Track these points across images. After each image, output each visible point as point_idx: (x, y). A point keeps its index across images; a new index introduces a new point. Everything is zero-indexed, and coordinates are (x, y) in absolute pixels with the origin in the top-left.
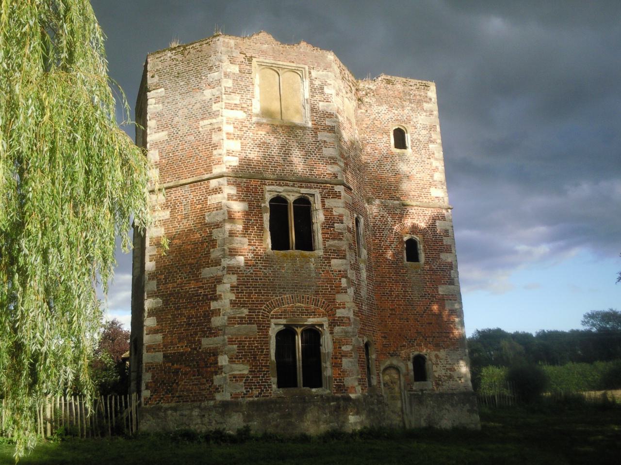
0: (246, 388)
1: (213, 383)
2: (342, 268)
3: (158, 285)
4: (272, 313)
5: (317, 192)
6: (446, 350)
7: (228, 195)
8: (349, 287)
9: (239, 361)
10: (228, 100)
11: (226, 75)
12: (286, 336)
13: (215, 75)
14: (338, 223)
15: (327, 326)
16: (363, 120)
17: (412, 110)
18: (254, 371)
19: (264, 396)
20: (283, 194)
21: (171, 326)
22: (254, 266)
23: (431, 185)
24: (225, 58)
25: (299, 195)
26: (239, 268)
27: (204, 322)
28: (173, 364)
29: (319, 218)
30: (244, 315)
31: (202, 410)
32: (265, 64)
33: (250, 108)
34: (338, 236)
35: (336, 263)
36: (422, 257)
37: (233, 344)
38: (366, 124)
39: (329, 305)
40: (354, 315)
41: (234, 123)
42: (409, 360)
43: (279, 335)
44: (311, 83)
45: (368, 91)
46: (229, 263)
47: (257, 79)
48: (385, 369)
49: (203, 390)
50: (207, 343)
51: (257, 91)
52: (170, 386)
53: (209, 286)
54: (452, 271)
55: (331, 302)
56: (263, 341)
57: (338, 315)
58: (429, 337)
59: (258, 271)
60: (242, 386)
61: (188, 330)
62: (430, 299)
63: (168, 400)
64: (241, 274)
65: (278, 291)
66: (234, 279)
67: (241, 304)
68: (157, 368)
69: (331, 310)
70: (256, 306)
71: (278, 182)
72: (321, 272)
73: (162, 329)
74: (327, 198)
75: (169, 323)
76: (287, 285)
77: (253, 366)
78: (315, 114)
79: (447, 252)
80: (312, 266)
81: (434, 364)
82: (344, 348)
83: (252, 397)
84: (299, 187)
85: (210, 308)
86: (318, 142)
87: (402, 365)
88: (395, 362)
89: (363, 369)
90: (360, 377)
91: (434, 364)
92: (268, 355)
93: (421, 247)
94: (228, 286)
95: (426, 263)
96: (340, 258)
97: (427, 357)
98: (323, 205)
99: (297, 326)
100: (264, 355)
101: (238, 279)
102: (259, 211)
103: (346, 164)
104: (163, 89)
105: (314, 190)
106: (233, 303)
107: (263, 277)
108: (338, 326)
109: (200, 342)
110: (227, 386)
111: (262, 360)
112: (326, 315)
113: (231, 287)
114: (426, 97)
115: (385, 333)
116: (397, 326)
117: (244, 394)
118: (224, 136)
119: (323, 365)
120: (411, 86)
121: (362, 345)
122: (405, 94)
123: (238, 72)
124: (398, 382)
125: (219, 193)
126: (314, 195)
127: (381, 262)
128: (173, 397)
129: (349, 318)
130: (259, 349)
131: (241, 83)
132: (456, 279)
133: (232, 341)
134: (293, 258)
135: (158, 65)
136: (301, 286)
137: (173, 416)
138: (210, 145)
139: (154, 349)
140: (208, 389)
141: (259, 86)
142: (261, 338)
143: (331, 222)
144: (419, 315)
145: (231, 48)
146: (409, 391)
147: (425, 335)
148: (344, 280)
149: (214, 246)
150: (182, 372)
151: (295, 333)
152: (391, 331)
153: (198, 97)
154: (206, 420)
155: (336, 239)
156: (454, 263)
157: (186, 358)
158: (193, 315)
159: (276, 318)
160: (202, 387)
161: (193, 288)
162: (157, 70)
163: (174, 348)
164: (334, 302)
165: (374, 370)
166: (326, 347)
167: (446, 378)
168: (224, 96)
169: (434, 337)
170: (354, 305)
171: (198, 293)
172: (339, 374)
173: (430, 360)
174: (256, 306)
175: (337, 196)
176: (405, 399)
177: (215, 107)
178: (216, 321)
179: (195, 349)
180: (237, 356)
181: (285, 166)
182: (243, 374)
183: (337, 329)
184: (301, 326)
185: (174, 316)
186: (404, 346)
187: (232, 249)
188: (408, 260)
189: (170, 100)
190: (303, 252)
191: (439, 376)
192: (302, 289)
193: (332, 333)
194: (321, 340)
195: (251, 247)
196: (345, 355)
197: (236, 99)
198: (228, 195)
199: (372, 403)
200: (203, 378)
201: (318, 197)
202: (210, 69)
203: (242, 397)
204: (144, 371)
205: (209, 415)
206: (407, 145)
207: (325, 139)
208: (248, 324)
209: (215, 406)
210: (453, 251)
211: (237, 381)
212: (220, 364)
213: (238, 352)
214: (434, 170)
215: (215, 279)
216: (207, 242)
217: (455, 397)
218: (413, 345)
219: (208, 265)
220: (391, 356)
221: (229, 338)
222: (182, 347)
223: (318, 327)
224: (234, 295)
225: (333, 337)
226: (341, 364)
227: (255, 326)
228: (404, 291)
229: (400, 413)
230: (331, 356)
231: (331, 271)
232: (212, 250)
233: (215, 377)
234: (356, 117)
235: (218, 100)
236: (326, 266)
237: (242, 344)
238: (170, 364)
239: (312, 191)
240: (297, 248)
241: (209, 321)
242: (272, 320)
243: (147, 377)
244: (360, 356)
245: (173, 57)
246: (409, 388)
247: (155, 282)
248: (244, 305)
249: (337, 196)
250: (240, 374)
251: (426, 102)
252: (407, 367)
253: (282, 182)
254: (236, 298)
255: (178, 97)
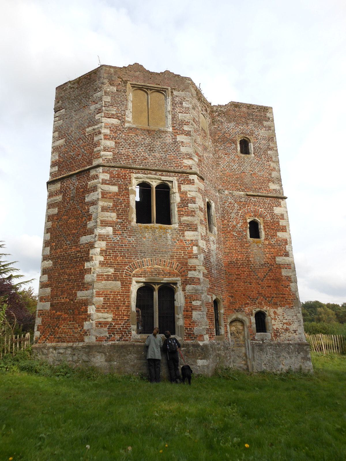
0: (109, 333)
1: (83, 328)
2: (194, 238)
3: (51, 250)
4: (134, 272)
5: (174, 179)
6: (283, 308)
7: (103, 180)
8: (200, 254)
9: (104, 311)
10: (107, 111)
11: (106, 93)
12: (145, 291)
13: (99, 94)
14: (191, 203)
15: (180, 284)
16: (216, 133)
17: (255, 127)
18: (117, 319)
19: (124, 340)
20: (148, 181)
21: (57, 282)
22: (120, 235)
23: (269, 181)
24: (106, 81)
25: (161, 181)
26: (108, 236)
27: (79, 279)
28: (56, 312)
29: (176, 198)
30: (110, 274)
31: (73, 349)
32: (137, 86)
33: (124, 117)
34: (192, 213)
35: (189, 235)
36: (263, 234)
37: (99, 297)
38: (219, 136)
39: (182, 268)
40: (203, 276)
41: (110, 128)
42: (252, 315)
43: (140, 290)
44: (173, 99)
45: (220, 112)
46: (100, 232)
47: (131, 97)
48: (231, 322)
49: (76, 333)
50: (81, 295)
51: (130, 105)
52: (54, 329)
53: (84, 250)
54: (287, 246)
55: (183, 265)
56: (125, 295)
57: (189, 276)
58: (268, 297)
59: (124, 239)
60: (105, 331)
61: (68, 285)
62: (269, 267)
63: (51, 340)
64: (110, 240)
65: (140, 255)
66: (103, 244)
67: (108, 264)
68: (46, 315)
69: (184, 271)
70: (120, 267)
71: (143, 171)
72: (176, 241)
73: (51, 285)
74: (183, 184)
75: (56, 280)
76: (147, 251)
77: (116, 315)
78: (175, 122)
79: (283, 232)
80: (169, 237)
81: (273, 319)
82: (194, 303)
83: (114, 340)
84: (160, 175)
85: (84, 267)
86: (177, 142)
87: (245, 319)
88: (240, 316)
89: (211, 321)
90: (208, 327)
91: (273, 319)
92: (129, 306)
93: (261, 227)
94: (98, 250)
95: (266, 239)
96: (192, 231)
97: (267, 313)
98: (180, 189)
99: (155, 283)
100: (126, 306)
101: (106, 245)
102: (127, 192)
103: (200, 160)
104: (64, 110)
105: (172, 178)
106: (102, 264)
107: (127, 243)
108: (190, 284)
109: (76, 294)
110: (93, 331)
111: (124, 310)
112: (179, 275)
113: (101, 251)
114: (266, 117)
115: (232, 293)
116: (242, 288)
117: (108, 338)
118: (102, 136)
119: (177, 316)
120: (253, 109)
121: (210, 301)
122: (249, 115)
123: (116, 91)
124: (243, 333)
125: (96, 179)
126: (172, 181)
127: (229, 238)
128: (55, 338)
129: (199, 279)
130: (122, 301)
131: (117, 99)
132: (290, 252)
133: (99, 294)
134: (153, 230)
135: (61, 93)
136: (159, 251)
137: (53, 354)
138: (92, 145)
139: (45, 299)
140: (79, 333)
141: (132, 102)
142: (123, 292)
143: (185, 202)
144: (260, 279)
145: (112, 74)
146: (252, 340)
147: (265, 295)
148: (195, 249)
149: (90, 219)
150: (62, 318)
151: (153, 290)
152: (236, 291)
153: (87, 111)
154: (75, 358)
155: (190, 215)
156: (288, 240)
157: (65, 307)
158: (72, 273)
159: (136, 277)
160: (76, 330)
161: (74, 252)
162: (61, 97)
163: (58, 299)
164: (186, 265)
165: (222, 323)
166: (179, 302)
167: (283, 330)
168: (104, 108)
169: (273, 297)
170: (204, 268)
171: (76, 256)
172: (190, 324)
173: (270, 316)
174: (120, 267)
175: (191, 182)
176: (248, 346)
177: (97, 117)
178: (88, 278)
179: (72, 300)
180: (103, 306)
181: (150, 160)
182: (107, 322)
183: (188, 287)
184: (158, 283)
185: (60, 274)
186: (248, 304)
187: (103, 221)
188: (251, 237)
189: (68, 116)
190: (162, 225)
191: (277, 328)
192: (160, 254)
193: (184, 290)
194: (175, 295)
195: (119, 220)
196: (195, 308)
197: (113, 111)
198: (103, 180)
199: (219, 349)
200: (76, 323)
201: (176, 184)
202: (95, 90)
203: (105, 341)
204: (37, 316)
205: (78, 354)
206: (250, 151)
207: (183, 140)
208: (113, 280)
209: (83, 347)
210: (288, 231)
211: (102, 326)
212: (89, 313)
213: (104, 303)
214: (272, 170)
215: (89, 245)
216: (85, 216)
217: (291, 346)
218: (255, 304)
219: (85, 234)
220: (237, 311)
221: (97, 292)
222: (63, 298)
223: (172, 285)
224: (103, 257)
225: (185, 293)
226: (191, 316)
227: (119, 283)
228: (247, 261)
229: (244, 358)
230: (183, 309)
231: (185, 240)
232: (88, 223)
233: (84, 323)
234: (210, 130)
235: (99, 111)
236: (180, 236)
237: (107, 297)
238: (54, 311)
239: (171, 179)
240: (157, 223)
241: (83, 278)
242: (133, 278)
243: (38, 321)
244: (209, 310)
245: (71, 86)
246: (251, 338)
247: (49, 248)
248: (111, 265)
249: (191, 182)
250: (105, 322)
251: (266, 121)
252: (251, 321)
253: (146, 171)
254: (105, 260)
255: (73, 114)
